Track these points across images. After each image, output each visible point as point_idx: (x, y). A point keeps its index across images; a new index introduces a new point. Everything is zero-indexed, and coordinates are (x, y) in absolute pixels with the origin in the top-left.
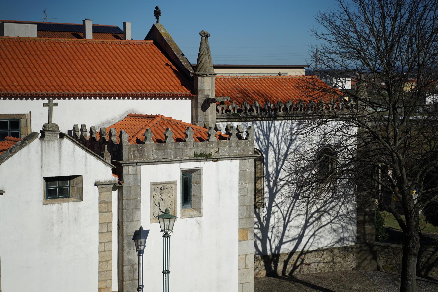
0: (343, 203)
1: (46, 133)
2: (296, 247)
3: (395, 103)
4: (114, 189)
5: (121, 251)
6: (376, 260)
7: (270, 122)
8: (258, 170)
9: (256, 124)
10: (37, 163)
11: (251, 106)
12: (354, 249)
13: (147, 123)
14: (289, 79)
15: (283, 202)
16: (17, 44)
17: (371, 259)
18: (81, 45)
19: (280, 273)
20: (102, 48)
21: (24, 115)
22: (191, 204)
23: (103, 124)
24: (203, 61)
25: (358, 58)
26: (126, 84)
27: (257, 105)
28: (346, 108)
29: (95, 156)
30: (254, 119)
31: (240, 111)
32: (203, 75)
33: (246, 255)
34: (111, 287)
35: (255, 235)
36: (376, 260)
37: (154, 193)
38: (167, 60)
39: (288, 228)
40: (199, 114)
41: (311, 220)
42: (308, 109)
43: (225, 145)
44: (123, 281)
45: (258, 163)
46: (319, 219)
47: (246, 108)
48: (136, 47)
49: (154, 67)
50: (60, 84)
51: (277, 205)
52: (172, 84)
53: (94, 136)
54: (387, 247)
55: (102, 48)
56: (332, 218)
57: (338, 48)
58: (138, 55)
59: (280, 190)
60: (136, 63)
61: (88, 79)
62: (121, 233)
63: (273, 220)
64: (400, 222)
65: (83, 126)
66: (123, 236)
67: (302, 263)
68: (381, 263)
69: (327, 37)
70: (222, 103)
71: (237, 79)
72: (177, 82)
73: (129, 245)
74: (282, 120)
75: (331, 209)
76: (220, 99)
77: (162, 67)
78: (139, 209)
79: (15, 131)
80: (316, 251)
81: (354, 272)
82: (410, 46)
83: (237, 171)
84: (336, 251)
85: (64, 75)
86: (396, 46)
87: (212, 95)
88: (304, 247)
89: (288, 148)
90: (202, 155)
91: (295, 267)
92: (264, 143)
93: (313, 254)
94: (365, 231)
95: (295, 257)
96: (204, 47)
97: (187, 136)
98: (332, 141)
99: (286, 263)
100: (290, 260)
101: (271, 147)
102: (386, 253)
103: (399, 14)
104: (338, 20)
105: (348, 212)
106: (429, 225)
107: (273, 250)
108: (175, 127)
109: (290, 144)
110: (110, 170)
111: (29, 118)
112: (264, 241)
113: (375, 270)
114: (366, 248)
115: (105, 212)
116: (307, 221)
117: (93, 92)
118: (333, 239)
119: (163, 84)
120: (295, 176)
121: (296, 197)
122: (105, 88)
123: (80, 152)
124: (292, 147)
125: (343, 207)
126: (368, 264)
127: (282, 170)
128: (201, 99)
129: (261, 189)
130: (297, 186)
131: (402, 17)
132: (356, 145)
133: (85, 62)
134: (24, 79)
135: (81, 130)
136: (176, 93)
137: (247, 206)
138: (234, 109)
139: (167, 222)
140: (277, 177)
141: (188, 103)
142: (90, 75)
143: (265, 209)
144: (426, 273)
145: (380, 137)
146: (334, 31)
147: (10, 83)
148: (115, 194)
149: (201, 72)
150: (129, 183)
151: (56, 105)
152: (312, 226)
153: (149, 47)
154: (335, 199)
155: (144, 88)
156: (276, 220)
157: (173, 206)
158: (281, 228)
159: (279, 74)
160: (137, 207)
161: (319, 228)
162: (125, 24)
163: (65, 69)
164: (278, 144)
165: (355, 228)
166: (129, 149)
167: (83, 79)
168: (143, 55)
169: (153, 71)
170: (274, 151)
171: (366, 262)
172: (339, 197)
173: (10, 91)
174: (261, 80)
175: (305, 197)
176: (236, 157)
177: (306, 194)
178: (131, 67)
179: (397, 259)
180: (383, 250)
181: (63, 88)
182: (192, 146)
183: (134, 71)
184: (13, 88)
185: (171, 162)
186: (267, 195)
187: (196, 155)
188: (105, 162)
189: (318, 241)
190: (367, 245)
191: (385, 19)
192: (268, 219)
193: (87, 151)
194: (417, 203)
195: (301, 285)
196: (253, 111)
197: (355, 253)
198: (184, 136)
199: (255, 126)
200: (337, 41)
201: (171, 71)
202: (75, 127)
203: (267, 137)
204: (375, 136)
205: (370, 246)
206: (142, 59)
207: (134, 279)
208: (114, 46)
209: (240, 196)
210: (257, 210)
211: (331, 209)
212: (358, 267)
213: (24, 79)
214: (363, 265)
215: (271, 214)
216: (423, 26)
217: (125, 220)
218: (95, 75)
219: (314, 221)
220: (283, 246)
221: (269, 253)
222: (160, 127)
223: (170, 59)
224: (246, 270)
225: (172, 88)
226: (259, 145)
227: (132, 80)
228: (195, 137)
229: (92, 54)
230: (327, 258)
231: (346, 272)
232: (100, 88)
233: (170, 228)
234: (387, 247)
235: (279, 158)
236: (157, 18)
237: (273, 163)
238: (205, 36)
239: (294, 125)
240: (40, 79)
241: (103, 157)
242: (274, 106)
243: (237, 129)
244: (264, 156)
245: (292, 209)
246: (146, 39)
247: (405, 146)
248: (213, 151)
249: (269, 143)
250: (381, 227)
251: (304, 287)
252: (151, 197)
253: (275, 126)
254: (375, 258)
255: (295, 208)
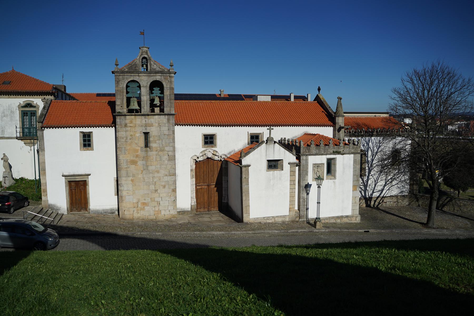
0: (403, 175)
1: (268, 141)
2: (380, 194)
3: (429, 130)
4: (297, 166)
5: (299, 193)
6: (418, 202)
7: (370, 137)
8: (363, 159)
9: (363, 138)
10: (264, 154)
11: (361, 130)
12: (408, 196)
13: (312, 137)
14: (379, 118)
15: (375, 174)
16: (259, 104)
17: (416, 201)
18: (286, 104)
19: (372, 206)
20: (294, 105)
21: (261, 133)
22: (331, 174)
23: (293, 137)
24: (339, 110)
25: (411, 109)
26: (304, 120)
27: (364, 130)
28: (406, 132)
29: (289, 151)
30: (362, 136)
31: (355, 132)
32: (338, 117)
33: (355, 197)
34: (295, 208)
35: (361, 188)
36: (418, 202)
37: (314, 168)
38: (322, 110)
39: (377, 186)
40: (336, 133)
41: (388, 183)
42: (388, 132)
43: (347, 148)
44: (300, 206)
45: (363, 156)
46: (391, 182)
47: (358, 131)
48: (309, 104)
49: (317, 113)
50: (276, 120)
51: (372, 175)
52: (325, 120)
53: (289, 142)
54: (424, 196)
55: (294, 105)
56: (398, 182)
57: (401, 104)
58: (310, 107)
59: (373, 168)
60: (309, 111)
61: (288, 118)
62: (299, 185)
63: (369, 182)
64: (429, 184)
65: (285, 138)
66: (300, 186)
67: (383, 202)
68: (420, 203)
69: (396, 99)
70: (347, 129)
71: (355, 118)
72: (327, 119)
73: (303, 190)
74: (375, 137)
75: (398, 178)
76: (346, 127)
77: (320, 113)
78: (307, 175)
79: (257, 140)
80: (390, 196)
81: (407, 206)
82: (436, 103)
83: (353, 160)
84: (399, 197)
85: (278, 116)
86: (429, 103)
87: (343, 125)
88: (384, 195)
89: (378, 150)
90: (336, 152)
91: (379, 203)
92: (366, 147)
93: (388, 198)
94: (413, 188)
95: (379, 199)
96: (339, 104)
97: (330, 143)
98: (399, 147)
99: (375, 201)
100: (377, 200)
101: (370, 149)
102: (423, 199)
103: (431, 88)
104: (402, 91)
105: (405, 180)
106: (445, 186)
107: (369, 196)
108: (324, 139)
109: (379, 148)
110: (295, 157)
111: (263, 135)
112: (365, 190)
113: (417, 206)
114: (414, 196)
115: (293, 176)
116: (386, 183)
117: (289, 124)
118: (398, 191)
119: (321, 120)
120: (381, 163)
121: (381, 172)
122: (295, 122)
123: (282, 149)
124: (380, 149)
125: (403, 177)
126: (414, 203)
127: (374, 160)
128: (337, 127)
129: (365, 168)
130: (382, 167)
131: (432, 90)
132: (410, 149)
133: (287, 111)
134: (261, 118)
135: (284, 140)
136: (326, 124)
137: (357, 176)
138: (353, 131)
139: (319, 181)
140: (372, 163)
141: (331, 129)
142: (288, 116)
143: (366, 177)
144: (442, 208)
145: (421, 145)
146: (400, 96)
147: (255, 120)
148: (297, 168)
149: (337, 115)
150: (303, 163)
151: (273, 129)
152: (388, 185)
153: (315, 104)
154: (400, 173)
155: (312, 122)
156: (371, 182)
157: (323, 174)
158: (374, 186)
159: (375, 116)
160: (307, 174)
161: (391, 186)
162: (308, 94)
163: (278, 114)
164: (373, 147)
165: (409, 187)
166: (304, 148)
167: (285, 118)
168: (312, 107)
169: (316, 114)
170: (371, 151)
171: (413, 202)
172: (402, 173)
173: (255, 124)
174: (366, 119)
175: (385, 172)
176: (352, 153)
177: (386, 171)
178: (306, 113)
179: (428, 202)
180: (422, 197)
181: (277, 122)
182: (332, 148)
183: (308, 114)
184: (257, 122)
185: (322, 154)
186: (367, 171)
187: (334, 152)
188: (293, 154)
189: (391, 192)
190: (414, 194)
191: (424, 90)
192: (367, 182)
193: (285, 149)
194: (438, 176)
195: (381, 211)
196: (362, 133)
197: (408, 199)
198: (328, 143)
199: (362, 139)
200: (401, 101)
201: (324, 114)
202: (282, 139)
203: (368, 144)
204: (419, 145)
205: (416, 195)
206: (311, 109)
207: (305, 205)
208: (299, 104)
209: (353, 171)
210: (362, 177)
211: (398, 178)
212: (409, 205)
213: (261, 118)
214: (412, 204)
215: (369, 179)
216: (443, 94)
217: (301, 179)
218: (291, 116)
219: (389, 183)
220: (374, 194)
221: (367, 197)
222: (318, 139)
223: (324, 109)
224: (355, 204)
225: (324, 122)
226: (364, 148)
227: (307, 118)
228: (334, 144)
229: (290, 107)
230: (394, 200)
231: (403, 207)
232: (293, 122)
233: (321, 184)
234: (424, 196)
235: (373, 154)
236: (319, 92)
237: (370, 156)
238: (340, 99)
239: (381, 139)
240: (268, 118)
241: (292, 152)
242: (372, 130)
243: (353, 141)
244: (366, 153)
245: (379, 178)
246: (314, 101)
247: (433, 150)
248: (341, 150)
249: (369, 147)
250: (422, 186)
251: (383, 212)
252: (313, 170)
253: (372, 140)
254: (418, 201)
255: (380, 177)
